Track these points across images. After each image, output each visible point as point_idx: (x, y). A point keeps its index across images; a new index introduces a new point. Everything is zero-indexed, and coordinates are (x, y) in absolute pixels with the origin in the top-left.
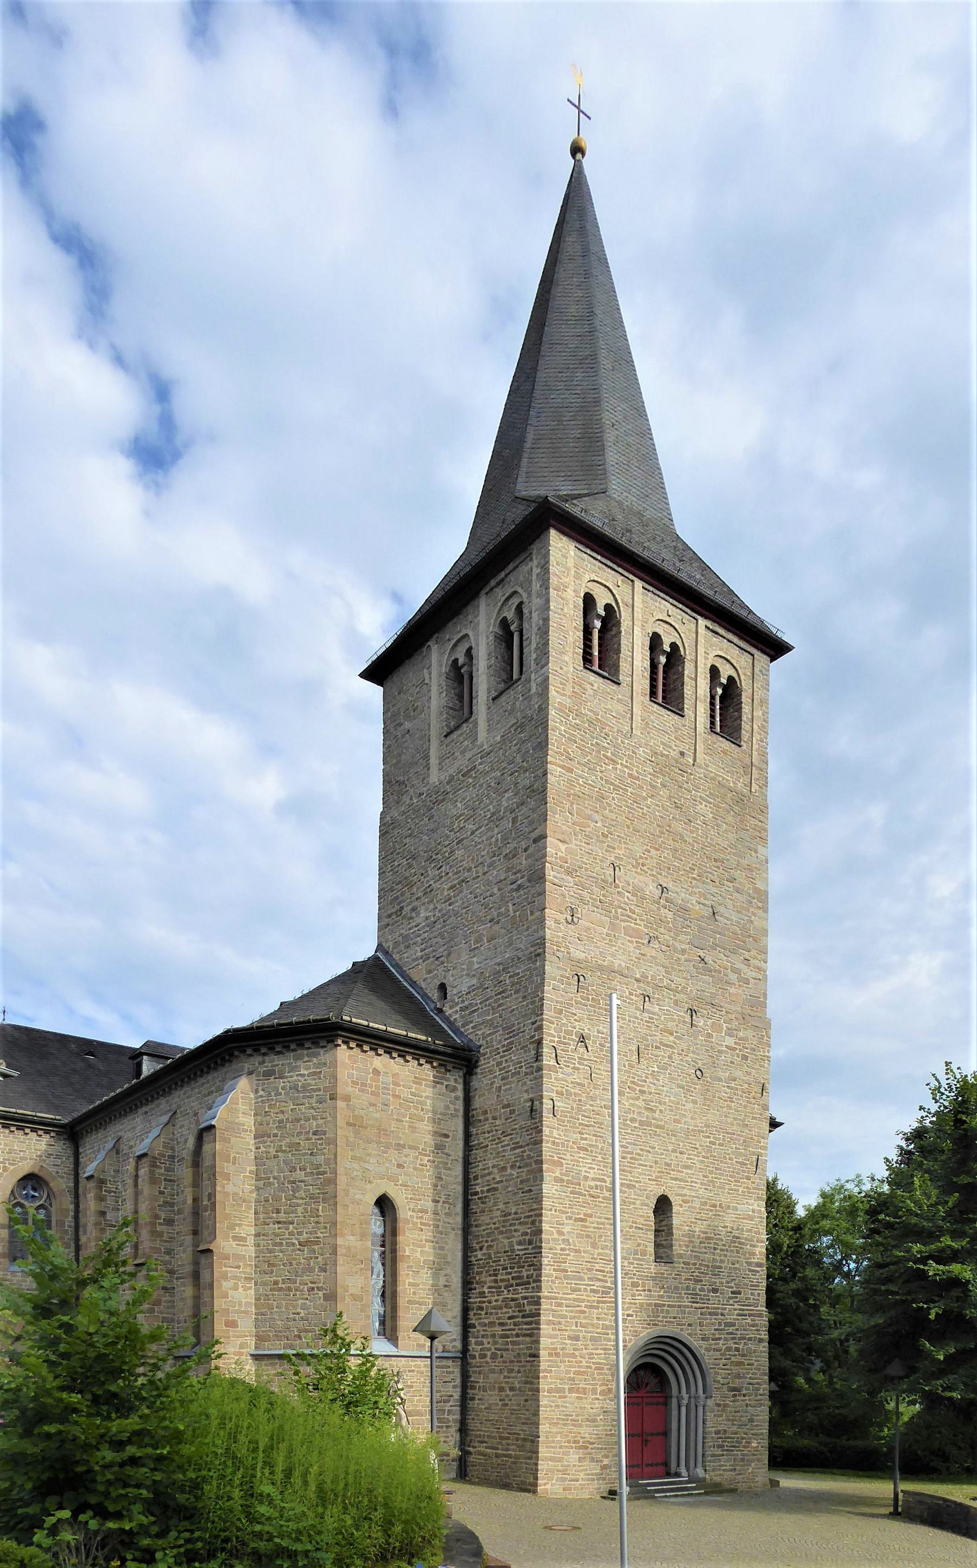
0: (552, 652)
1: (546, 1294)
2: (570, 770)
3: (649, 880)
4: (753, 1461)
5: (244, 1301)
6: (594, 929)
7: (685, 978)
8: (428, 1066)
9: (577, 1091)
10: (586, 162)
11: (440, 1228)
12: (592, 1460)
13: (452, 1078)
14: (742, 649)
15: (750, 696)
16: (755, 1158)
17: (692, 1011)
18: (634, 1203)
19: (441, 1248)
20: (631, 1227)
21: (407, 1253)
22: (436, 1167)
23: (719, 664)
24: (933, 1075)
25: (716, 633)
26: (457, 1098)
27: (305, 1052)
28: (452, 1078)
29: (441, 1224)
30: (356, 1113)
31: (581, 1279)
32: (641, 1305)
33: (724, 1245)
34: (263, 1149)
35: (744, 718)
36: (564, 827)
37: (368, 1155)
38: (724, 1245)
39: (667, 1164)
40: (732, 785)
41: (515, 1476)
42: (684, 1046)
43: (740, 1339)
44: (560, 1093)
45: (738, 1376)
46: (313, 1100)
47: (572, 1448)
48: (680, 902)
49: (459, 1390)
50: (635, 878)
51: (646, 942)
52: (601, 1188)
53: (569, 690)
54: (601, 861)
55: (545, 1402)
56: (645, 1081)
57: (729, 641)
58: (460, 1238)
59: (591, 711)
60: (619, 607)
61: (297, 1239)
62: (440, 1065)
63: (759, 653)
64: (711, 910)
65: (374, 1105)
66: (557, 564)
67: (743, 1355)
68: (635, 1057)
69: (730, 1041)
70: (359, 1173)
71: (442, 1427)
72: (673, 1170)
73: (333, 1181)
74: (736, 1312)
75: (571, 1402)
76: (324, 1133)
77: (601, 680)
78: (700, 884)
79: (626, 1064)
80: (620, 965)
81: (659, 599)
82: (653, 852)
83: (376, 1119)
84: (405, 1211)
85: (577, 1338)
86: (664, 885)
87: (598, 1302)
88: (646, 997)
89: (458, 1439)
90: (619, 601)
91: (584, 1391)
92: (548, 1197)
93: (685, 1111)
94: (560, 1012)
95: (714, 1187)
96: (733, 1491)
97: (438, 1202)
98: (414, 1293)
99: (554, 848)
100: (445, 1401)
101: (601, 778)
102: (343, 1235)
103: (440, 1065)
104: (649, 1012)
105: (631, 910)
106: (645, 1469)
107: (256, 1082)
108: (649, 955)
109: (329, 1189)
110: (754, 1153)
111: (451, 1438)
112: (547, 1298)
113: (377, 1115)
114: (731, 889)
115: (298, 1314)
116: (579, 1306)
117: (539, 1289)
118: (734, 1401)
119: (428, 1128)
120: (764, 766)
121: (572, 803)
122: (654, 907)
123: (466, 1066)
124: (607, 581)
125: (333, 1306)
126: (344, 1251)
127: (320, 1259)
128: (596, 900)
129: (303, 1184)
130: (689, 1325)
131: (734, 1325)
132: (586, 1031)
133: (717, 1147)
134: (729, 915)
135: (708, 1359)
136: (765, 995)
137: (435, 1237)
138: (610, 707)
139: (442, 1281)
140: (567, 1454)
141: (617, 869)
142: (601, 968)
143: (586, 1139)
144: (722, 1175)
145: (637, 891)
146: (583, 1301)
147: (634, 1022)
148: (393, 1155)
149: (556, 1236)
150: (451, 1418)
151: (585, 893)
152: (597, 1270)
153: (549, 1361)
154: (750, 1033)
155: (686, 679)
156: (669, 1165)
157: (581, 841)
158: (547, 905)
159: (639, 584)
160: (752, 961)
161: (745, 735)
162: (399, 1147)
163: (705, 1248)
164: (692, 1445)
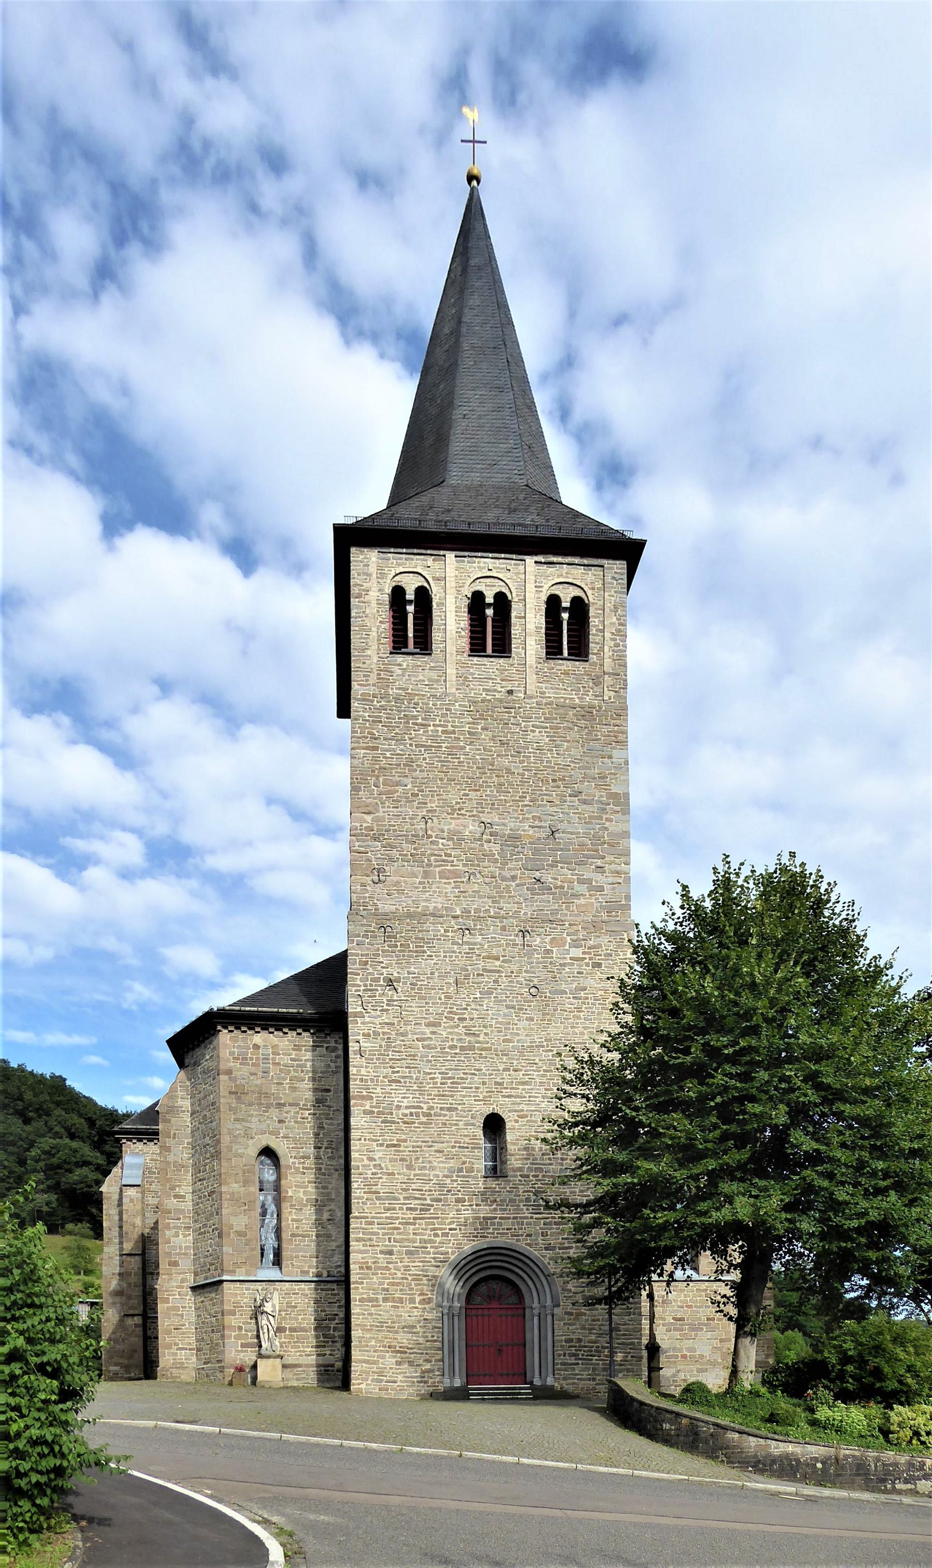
1: (357, 1214)
5: (183, 1245)
6: (405, 882)
7: (517, 903)
8: (308, 1034)
11: (323, 1171)
12: (411, 1363)
17: (524, 933)
18: (456, 1125)
20: (453, 1147)
21: (290, 1194)
22: (318, 1118)
26: (337, 1057)
30: (238, 1082)
31: (395, 1199)
32: (466, 1219)
39: (496, 1083)
40: (577, 701)
42: (515, 968)
44: (366, 1035)
47: (388, 1352)
49: (344, 1309)
52: (417, 1115)
53: (373, 678)
54: (411, 819)
59: (399, 689)
65: (256, 1074)
66: (359, 575)
69: (577, 952)
70: (241, 1132)
71: (328, 1342)
75: (386, 1310)
79: (443, 996)
81: (477, 560)
82: (472, 795)
83: (256, 1086)
84: (287, 1158)
85: (391, 1253)
91: (401, 1300)
94: (366, 963)
97: (320, 1148)
98: (297, 1228)
100: (330, 1320)
101: (411, 745)
102: (227, 1184)
108: (470, 890)
111: (337, 1352)
112: (357, 1218)
113: (259, 1082)
122: (476, 845)
128: (406, 855)
130: (527, 1235)
132: (396, 975)
136: (628, 898)
137: (317, 1178)
138: (421, 678)
139: (326, 1216)
140: (384, 1357)
142: (410, 915)
143: (398, 1072)
145: (456, 838)
146: (397, 1218)
148: (274, 1113)
149: (366, 1162)
150: (336, 1334)
156: (501, 1084)
157: (389, 807)
163: (550, 1159)
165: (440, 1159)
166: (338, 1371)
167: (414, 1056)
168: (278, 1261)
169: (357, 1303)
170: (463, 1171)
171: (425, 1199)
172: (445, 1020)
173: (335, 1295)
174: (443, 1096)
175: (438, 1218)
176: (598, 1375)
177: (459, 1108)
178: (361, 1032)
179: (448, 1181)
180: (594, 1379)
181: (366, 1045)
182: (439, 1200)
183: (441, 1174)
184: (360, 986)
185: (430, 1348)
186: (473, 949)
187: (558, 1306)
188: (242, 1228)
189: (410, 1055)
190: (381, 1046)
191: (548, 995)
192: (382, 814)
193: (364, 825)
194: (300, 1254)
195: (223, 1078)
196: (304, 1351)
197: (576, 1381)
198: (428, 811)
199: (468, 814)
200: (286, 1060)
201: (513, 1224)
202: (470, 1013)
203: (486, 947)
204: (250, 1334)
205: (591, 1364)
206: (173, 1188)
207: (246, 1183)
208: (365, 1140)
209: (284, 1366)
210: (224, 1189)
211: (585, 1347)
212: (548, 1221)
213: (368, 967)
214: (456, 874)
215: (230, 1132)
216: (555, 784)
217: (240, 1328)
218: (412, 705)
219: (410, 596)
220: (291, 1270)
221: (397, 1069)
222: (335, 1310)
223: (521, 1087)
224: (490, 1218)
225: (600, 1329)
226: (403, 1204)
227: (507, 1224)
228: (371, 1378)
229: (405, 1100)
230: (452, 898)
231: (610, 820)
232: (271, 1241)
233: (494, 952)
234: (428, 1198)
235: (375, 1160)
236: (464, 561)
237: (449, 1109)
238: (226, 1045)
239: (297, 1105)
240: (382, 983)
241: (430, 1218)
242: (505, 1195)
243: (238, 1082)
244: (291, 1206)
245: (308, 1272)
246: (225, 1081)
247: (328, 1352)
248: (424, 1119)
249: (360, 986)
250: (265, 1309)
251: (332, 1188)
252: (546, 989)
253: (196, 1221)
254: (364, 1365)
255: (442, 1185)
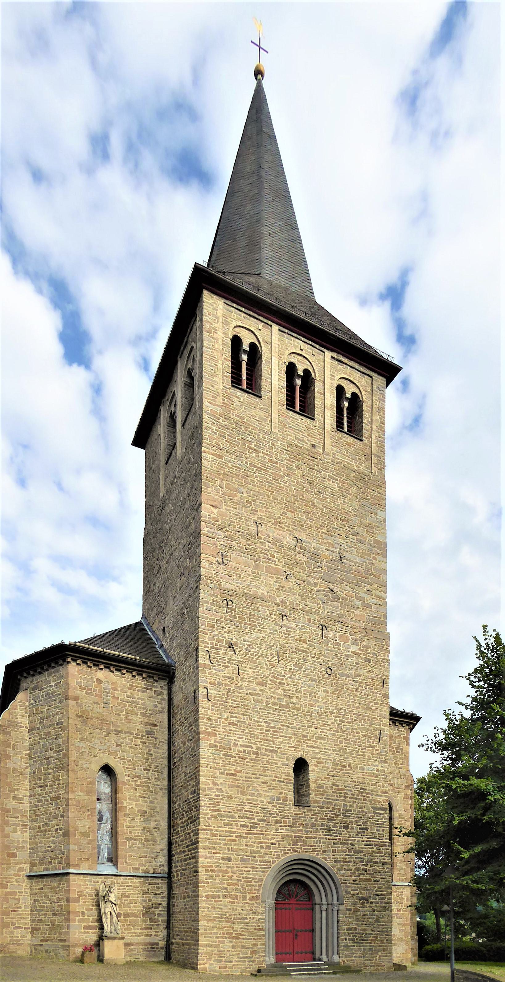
0: (205, 376)
1: (203, 827)
2: (220, 457)
3: (287, 534)
4: (379, 951)
5: (21, 840)
8: (139, 678)
9: (227, 682)
10: (265, 83)
11: (151, 789)
13: (159, 686)
14: (363, 373)
15: (370, 406)
16: (378, 732)
17: (323, 627)
18: (276, 763)
19: (152, 802)
20: (274, 780)
21: (125, 805)
23: (344, 384)
24: (475, 637)
25: (341, 362)
26: (163, 700)
27: (53, 670)
28: (159, 686)
29: (151, 785)
30: (84, 708)
31: (232, 817)
33: (352, 794)
34: (33, 738)
35: (365, 421)
36: (216, 497)
37: (93, 737)
38: (352, 794)
39: (303, 736)
40: (355, 468)
41: (189, 959)
42: (316, 651)
43: (367, 862)
45: (366, 889)
46: (57, 702)
47: (226, 938)
48: (312, 549)
49: (166, 900)
50: (274, 532)
51: (284, 577)
52: (249, 752)
53: (219, 400)
54: (246, 520)
55: (204, 905)
56: (284, 676)
57: (351, 367)
58: (166, 796)
59: (238, 416)
60: (261, 346)
61: (49, 796)
62: (149, 677)
63: (376, 375)
64: (338, 555)
67: (369, 874)
68: (275, 659)
69: (355, 648)
71: (153, 925)
72: (309, 740)
73: (66, 756)
74: (363, 843)
76: (62, 723)
77: (246, 395)
78: (329, 537)
79: (268, 663)
80: (263, 593)
81: (293, 338)
82: (289, 514)
83: (99, 713)
85: (229, 859)
86: (299, 537)
87: (247, 834)
88: (284, 616)
89: (166, 934)
90: (261, 340)
91: (236, 897)
92: (204, 758)
93: (318, 697)
95: (344, 752)
96: (358, 971)
98: (130, 833)
99: (207, 511)
100: (155, 908)
101: (246, 463)
102: (73, 792)
103: (148, 676)
104: (286, 626)
105: (271, 555)
106: (296, 956)
107: (29, 695)
109: (65, 761)
110: (377, 729)
111: (160, 933)
112: (204, 830)
113: (101, 711)
114: (355, 541)
115: (50, 847)
116: (231, 836)
117: (198, 824)
118: (362, 907)
119: (140, 720)
120: (381, 455)
121: (222, 480)
122: (291, 553)
123: (168, 677)
124: (251, 326)
125: (67, 840)
126: (75, 803)
127: (61, 809)
128: (242, 548)
129: (52, 759)
131: (362, 852)
132: (235, 640)
133: (346, 724)
134: (353, 558)
135: (339, 876)
138: (254, 413)
139: (153, 825)
140: (223, 942)
141: (259, 526)
142: (246, 596)
143: (235, 717)
144: (351, 744)
146: (234, 832)
147: (274, 634)
148: (113, 737)
149: (211, 786)
150: (160, 919)
151: (233, 543)
152: (245, 811)
153: (205, 875)
154: (372, 643)
155: (316, 394)
157: (230, 506)
158: (202, 551)
159: (275, 328)
160: (373, 592)
161: (366, 433)
162: (118, 732)
163: (337, 796)
164: (330, 939)
165: (265, 789)
166: (161, 948)
167: (247, 706)
168: (113, 860)
169: (204, 898)
170: (280, 799)
171: (254, 819)
172: (269, 682)
173: (159, 888)
174: (267, 740)
175: (263, 834)
176: (367, 953)
177: (278, 750)
178: (209, 681)
179: (270, 806)
180: (364, 957)
181: (212, 692)
182: (264, 821)
183: (265, 801)
184: (208, 644)
185: (257, 935)
186: (290, 631)
187: (343, 904)
188: (85, 830)
189: (244, 705)
190: (223, 694)
191: (338, 675)
192: (225, 511)
193: (212, 515)
194: (133, 854)
195: (71, 702)
196: (135, 933)
197: (353, 958)
198: (259, 518)
199: (286, 528)
200: (123, 696)
201: (314, 842)
202: (287, 680)
203: (298, 632)
204: (91, 918)
205: (363, 946)
206: (12, 791)
207: (89, 793)
208: (210, 768)
209: (126, 945)
210: (71, 796)
211: (359, 933)
212: (336, 841)
213: (214, 629)
214: (278, 572)
215: (77, 749)
216: (342, 523)
217: (83, 914)
218: (247, 432)
219: (246, 347)
220: (124, 868)
221: (235, 715)
222: (160, 900)
223: (319, 741)
224: (298, 837)
225: (368, 921)
226: (238, 821)
227: (310, 842)
228: (213, 959)
229: (240, 740)
230: (275, 590)
231: (376, 559)
232: (106, 842)
233: (304, 636)
234: (256, 818)
235: (218, 785)
236: (284, 336)
237: (271, 751)
238: (73, 675)
239: (131, 733)
240: (224, 644)
241: (257, 834)
242: (308, 820)
243: (84, 708)
244: (125, 814)
245: (138, 869)
246: (73, 706)
247: (153, 934)
248: (254, 757)
249: (208, 644)
250: (110, 899)
251: (157, 803)
252: (336, 671)
253: (33, 821)
254: (208, 948)
255: (266, 809)
